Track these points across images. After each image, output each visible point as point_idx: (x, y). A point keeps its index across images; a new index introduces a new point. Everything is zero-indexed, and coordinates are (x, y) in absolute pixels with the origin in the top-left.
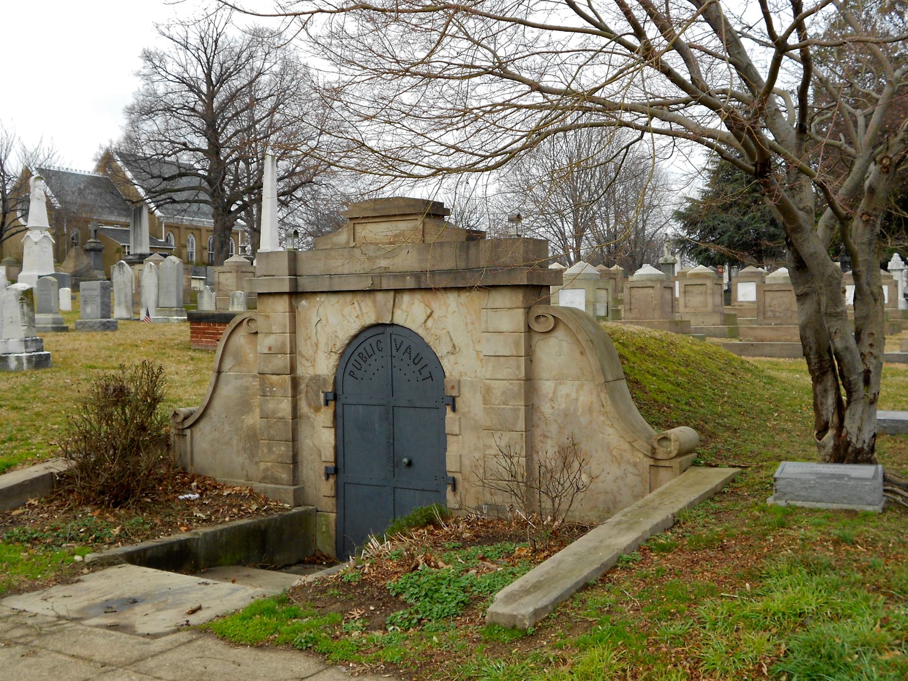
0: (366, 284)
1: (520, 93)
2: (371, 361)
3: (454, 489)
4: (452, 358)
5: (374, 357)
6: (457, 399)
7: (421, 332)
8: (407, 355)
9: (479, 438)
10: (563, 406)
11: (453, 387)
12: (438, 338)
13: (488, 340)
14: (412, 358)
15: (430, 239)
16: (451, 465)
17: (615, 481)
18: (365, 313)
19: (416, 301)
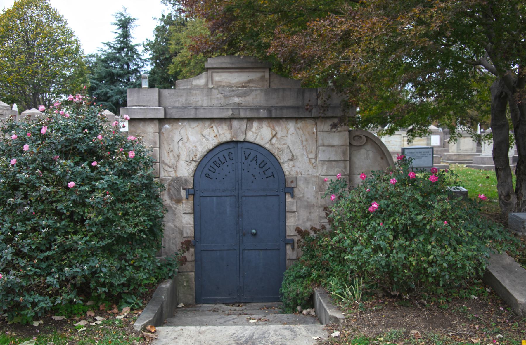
0: (228, 114)
1: (210, 79)
4: (291, 163)
5: (226, 164)
6: (295, 189)
7: (267, 146)
9: (310, 213)
11: (292, 182)
12: (281, 150)
13: (324, 151)
14: (258, 164)
15: (273, 86)
18: (223, 133)
19: (264, 126)
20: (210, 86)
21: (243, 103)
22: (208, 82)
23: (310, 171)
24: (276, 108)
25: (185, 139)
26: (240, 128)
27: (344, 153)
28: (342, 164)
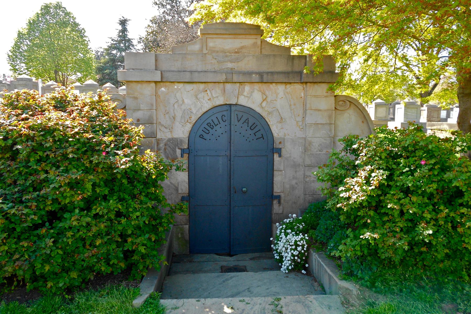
2: (217, 128)
3: (279, 202)
5: (219, 126)
7: (258, 109)
9: (296, 172)
11: (280, 143)
16: (277, 189)
20: (205, 51)
24: (268, 73)
25: (180, 102)
27: (330, 117)
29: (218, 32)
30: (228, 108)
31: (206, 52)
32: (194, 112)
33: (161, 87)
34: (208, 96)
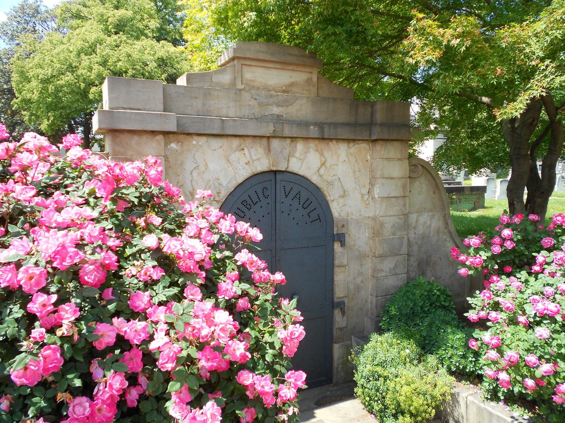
0: (268, 130)
4: (341, 201)
7: (315, 179)
8: (296, 200)
10: (421, 231)
11: (343, 226)
12: (330, 184)
13: (383, 184)
14: (302, 203)
16: (339, 292)
17: (450, 278)
20: (240, 86)
21: (284, 116)
22: (235, 78)
23: (362, 211)
24: (330, 124)
25: (202, 168)
26: (281, 152)
27: (404, 187)
28: (401, 201)
29: (261, 56)
30: (272, 176)
31: (242, 87)
32: (224, 184)
33: (171, 143)
34: (246, 157)
